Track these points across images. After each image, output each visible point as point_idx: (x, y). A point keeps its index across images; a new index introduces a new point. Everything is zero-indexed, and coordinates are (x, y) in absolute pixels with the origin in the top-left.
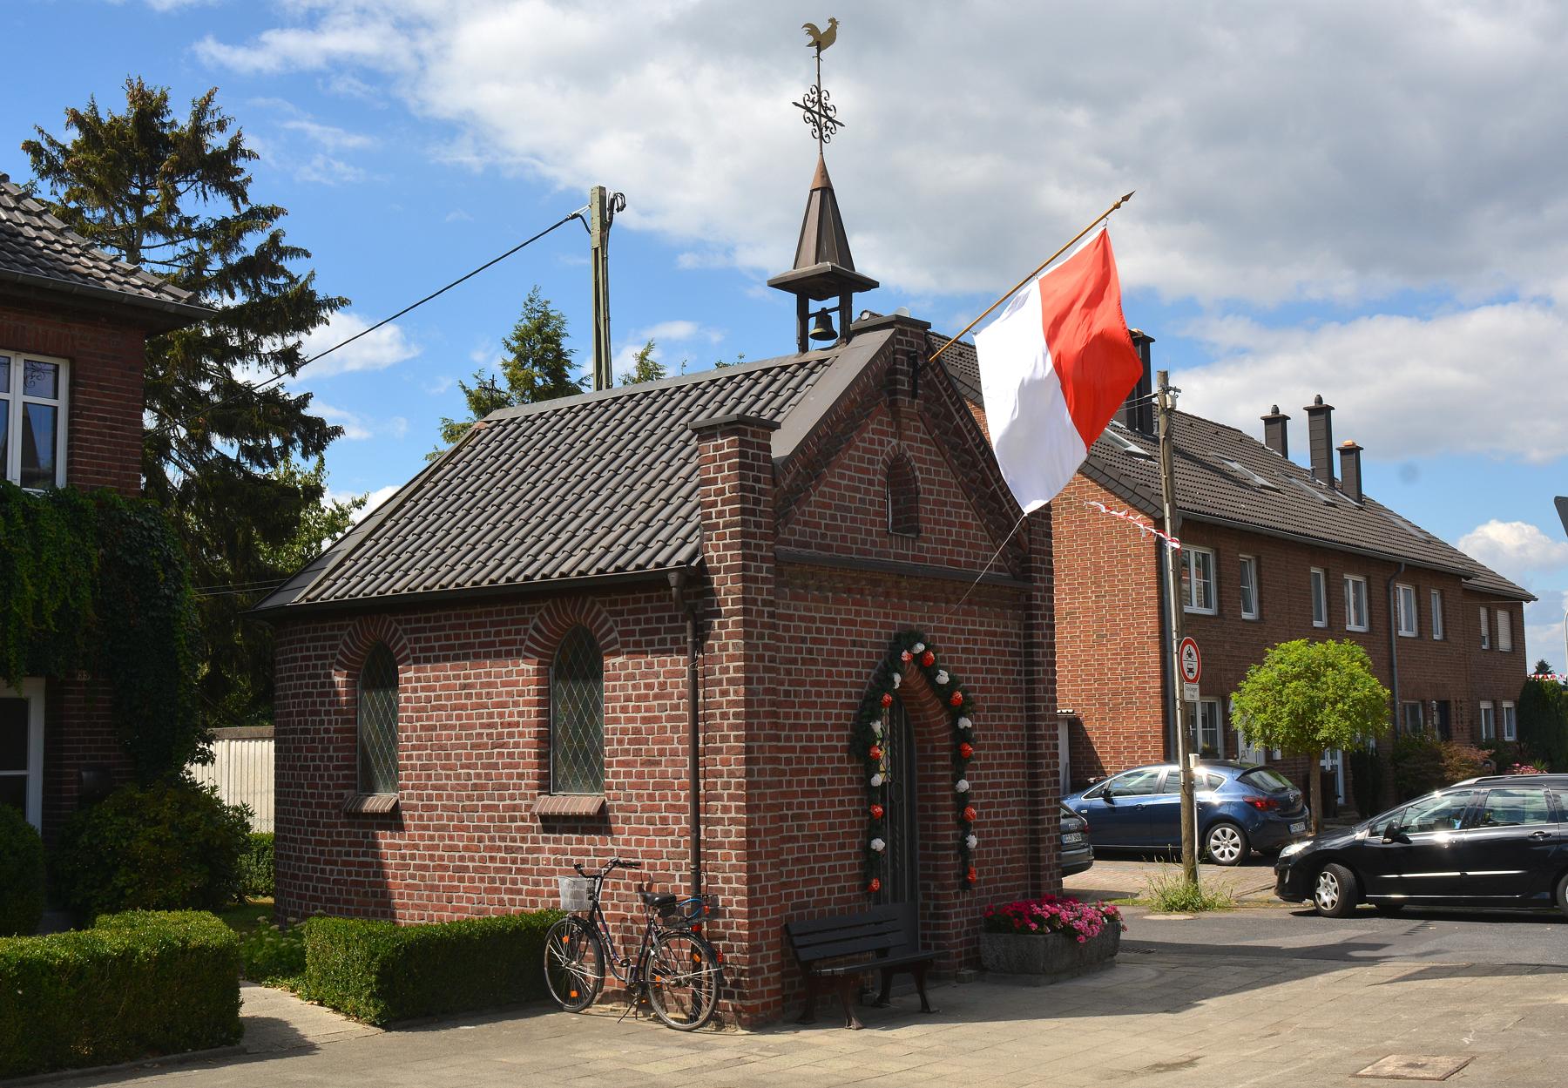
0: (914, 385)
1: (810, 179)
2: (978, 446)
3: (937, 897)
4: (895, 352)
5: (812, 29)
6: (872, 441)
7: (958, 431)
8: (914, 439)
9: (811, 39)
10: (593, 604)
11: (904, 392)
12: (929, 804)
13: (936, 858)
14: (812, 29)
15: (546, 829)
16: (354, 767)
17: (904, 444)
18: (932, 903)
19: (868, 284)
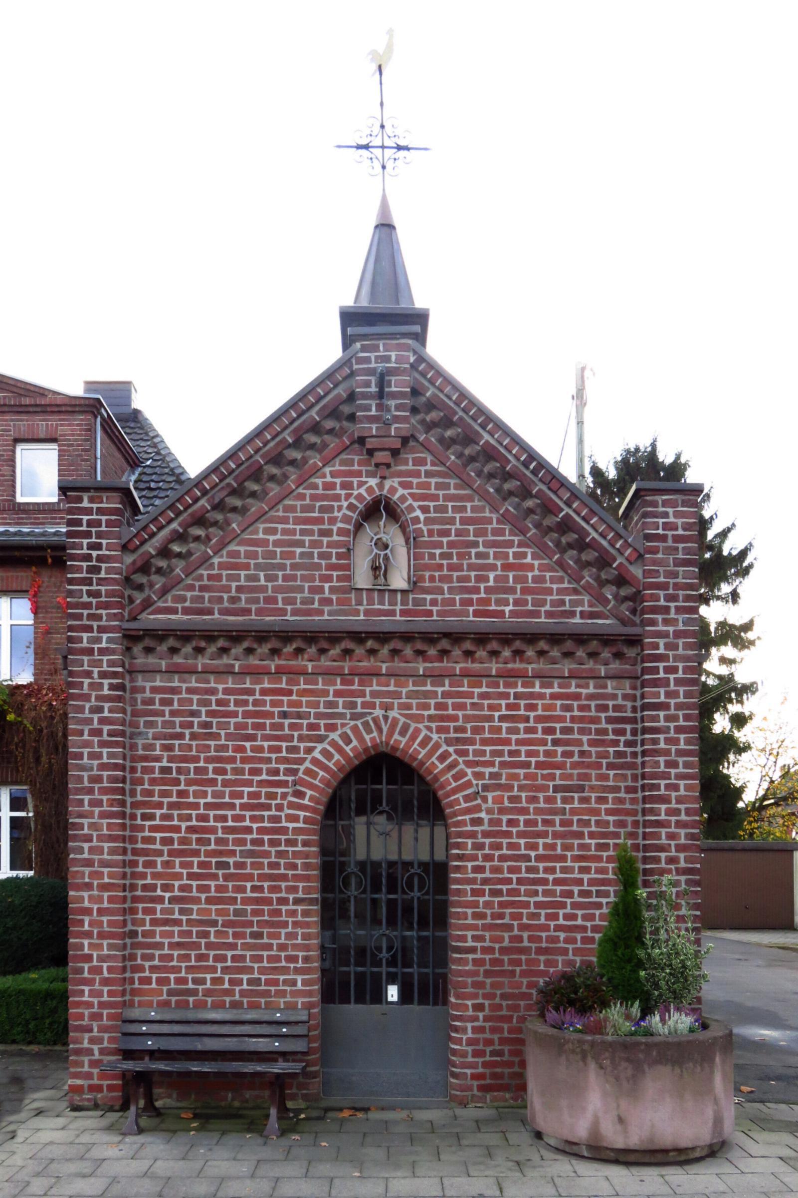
7: (489, 454)
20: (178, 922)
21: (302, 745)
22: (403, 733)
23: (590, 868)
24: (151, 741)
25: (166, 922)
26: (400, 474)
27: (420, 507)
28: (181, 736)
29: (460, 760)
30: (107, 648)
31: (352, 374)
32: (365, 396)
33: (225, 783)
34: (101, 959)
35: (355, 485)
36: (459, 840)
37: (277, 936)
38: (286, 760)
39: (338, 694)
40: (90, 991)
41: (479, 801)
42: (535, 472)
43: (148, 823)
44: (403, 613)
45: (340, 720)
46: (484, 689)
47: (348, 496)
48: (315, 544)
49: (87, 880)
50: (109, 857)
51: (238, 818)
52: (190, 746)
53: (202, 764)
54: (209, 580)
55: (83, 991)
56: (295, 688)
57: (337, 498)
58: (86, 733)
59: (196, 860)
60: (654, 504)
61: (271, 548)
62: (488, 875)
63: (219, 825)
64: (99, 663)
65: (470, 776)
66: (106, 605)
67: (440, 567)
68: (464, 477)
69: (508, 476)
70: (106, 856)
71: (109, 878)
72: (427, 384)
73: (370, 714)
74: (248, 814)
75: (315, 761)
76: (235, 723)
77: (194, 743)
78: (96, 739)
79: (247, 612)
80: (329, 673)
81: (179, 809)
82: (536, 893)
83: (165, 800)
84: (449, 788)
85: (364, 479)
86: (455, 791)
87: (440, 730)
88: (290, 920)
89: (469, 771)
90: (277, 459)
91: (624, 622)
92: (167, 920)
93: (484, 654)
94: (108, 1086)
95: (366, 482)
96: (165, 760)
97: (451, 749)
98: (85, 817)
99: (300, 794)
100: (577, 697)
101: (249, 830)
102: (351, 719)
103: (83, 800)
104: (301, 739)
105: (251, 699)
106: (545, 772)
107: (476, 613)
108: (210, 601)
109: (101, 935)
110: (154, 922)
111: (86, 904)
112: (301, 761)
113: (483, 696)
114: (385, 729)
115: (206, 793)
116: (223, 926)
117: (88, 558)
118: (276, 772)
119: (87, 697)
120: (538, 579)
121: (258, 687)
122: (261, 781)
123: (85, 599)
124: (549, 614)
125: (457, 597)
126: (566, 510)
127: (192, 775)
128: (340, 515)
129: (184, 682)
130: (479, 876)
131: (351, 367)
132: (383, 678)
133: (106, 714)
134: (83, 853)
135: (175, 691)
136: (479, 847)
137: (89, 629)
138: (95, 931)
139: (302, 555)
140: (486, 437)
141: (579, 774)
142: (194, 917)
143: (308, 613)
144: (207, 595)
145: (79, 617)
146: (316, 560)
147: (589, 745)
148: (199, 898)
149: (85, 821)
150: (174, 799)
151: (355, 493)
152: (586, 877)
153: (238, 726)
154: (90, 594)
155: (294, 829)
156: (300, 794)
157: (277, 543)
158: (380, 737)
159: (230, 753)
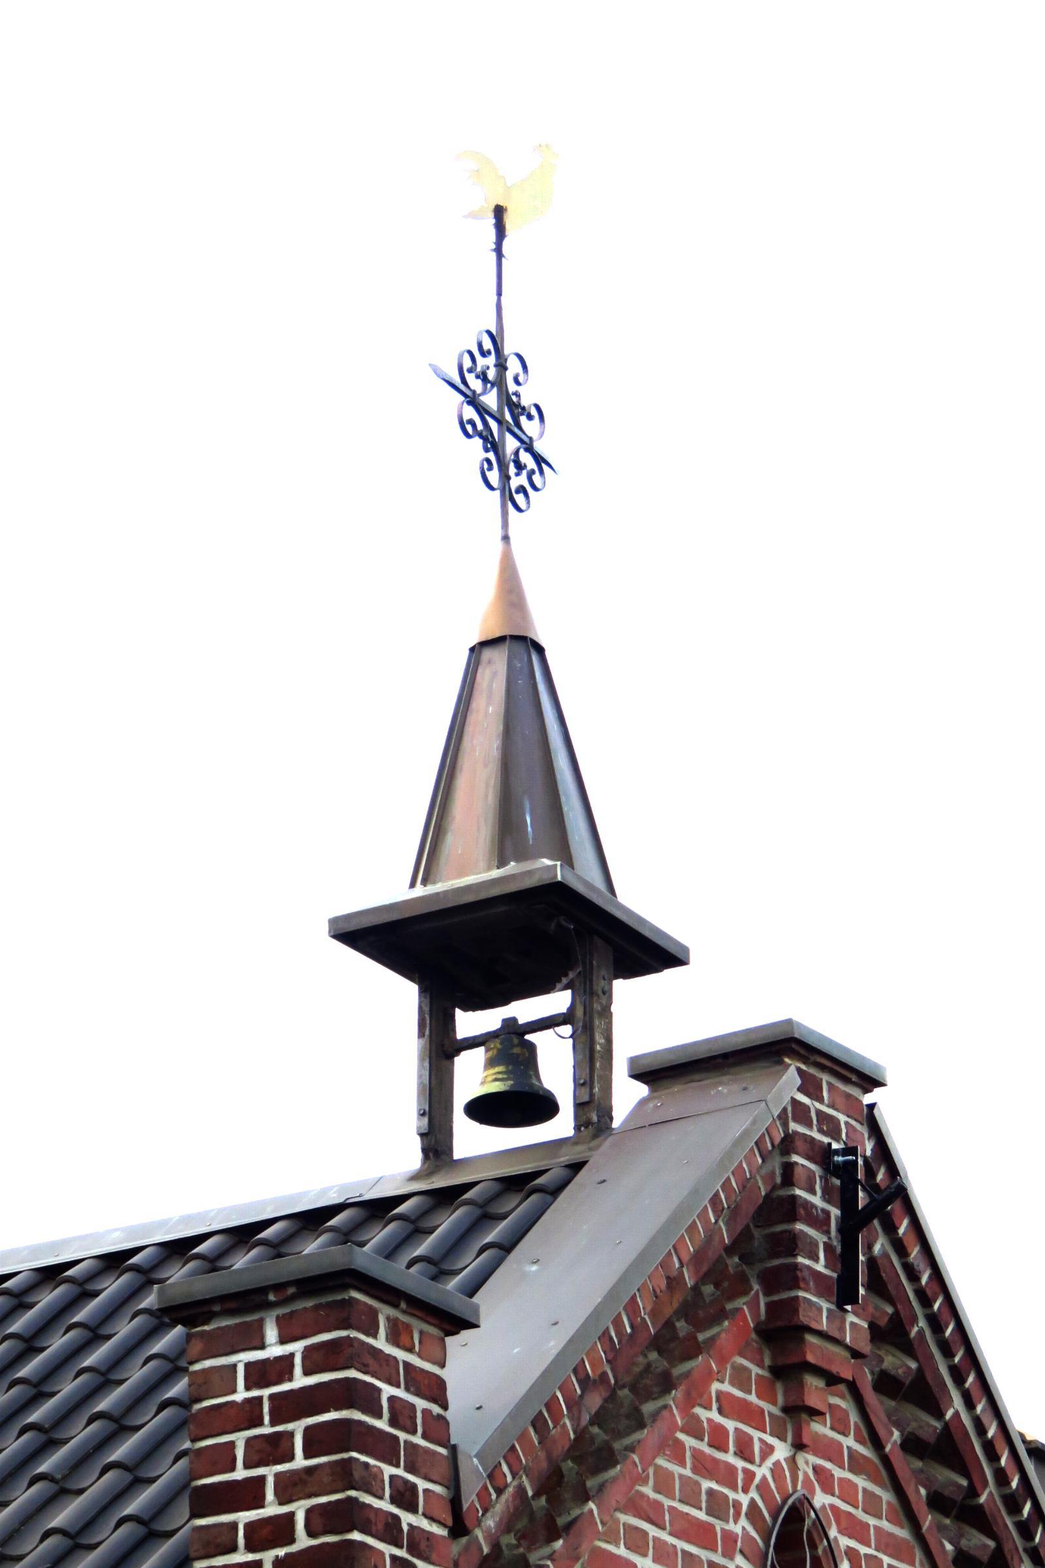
0: (845, 1259)
4: (788, 1144)
8: (831, 1452)
17: (808, 1461)
19: (649, 954)
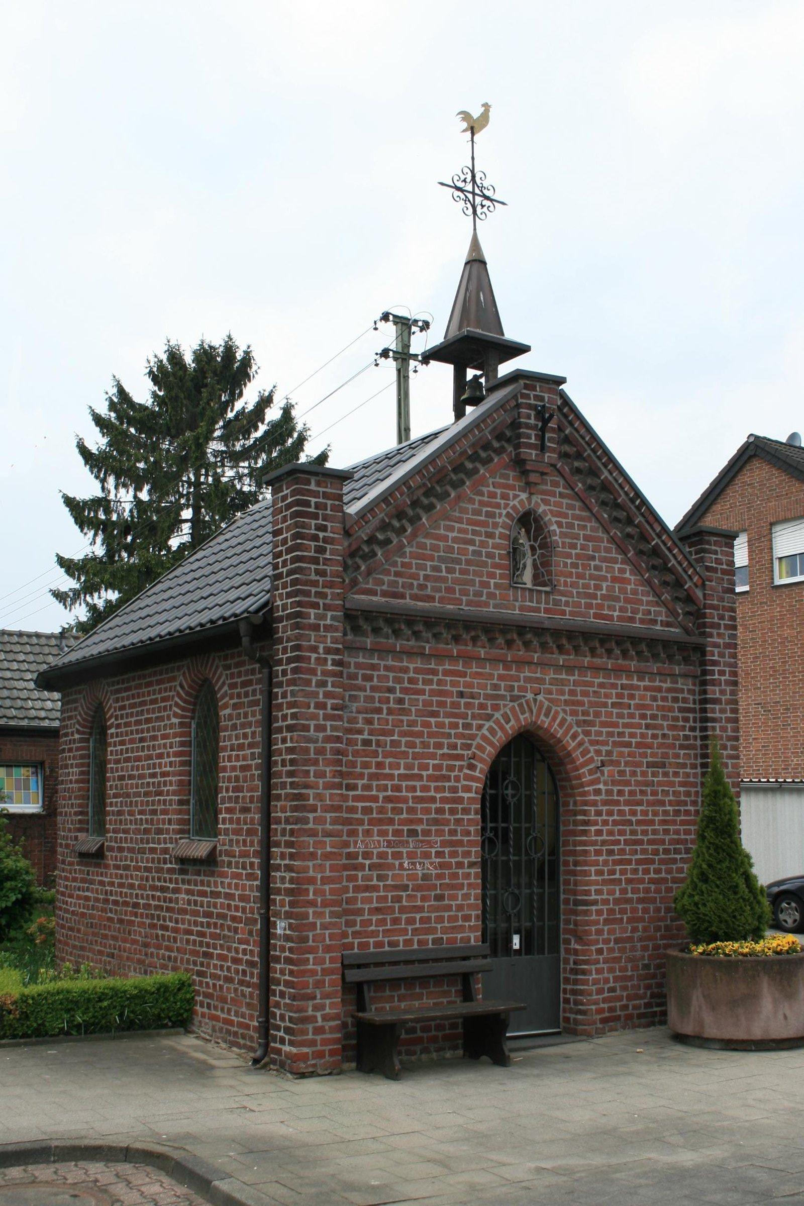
0: (542, 438)
1: (462, 254)
2: (632, 501)
3: (576, 952)
5: (466, 116)
6: (493, 495)
7: (605, 487)
9: (465, 125)
10: (214, 660)
11: (530, 446)
12: (571, 859)
13: (575, 913)
14: (466, 116)
15: (183, 872)
16: (86, 814)
18: (572, 958)
20: (375, 888)
21: (474, 723)
22: (547, 715)
23: (625, 831)
24: (354, 715)
25: (367, 888)
26: (543, 493)
27: (556, 522)
28: (379, 711)
29: (586, 739)
30: (331, 625)
31: (518, 406)
32: (528, 426)
33: (416, 756)
34: (324, 927)
35: (511, 497)
36: (586, 808)
37: (455, 897)
38: (462, 736)
39: (501, 678)
40: (314, 958)
41: (599, 774)
42: (638, 508)
43: (351, 793)
44: (547, 611)
45: (491, 702)
46: (601, 680)
47: (506, 505)
48: (483, 544)
49: (312, 850)
50: (331, 827)
51: (425, 789)
52: (387, 720)
53: (396, 737)
54: (402, 567)
55: (308, 959)
56: (469, 671)
57: (498, 506)
58: (312, 706)
59: (390, 828)
60: (709, 543)
61: (450, 543)
62: (605, 837)
63: (410, 795)
64: (323, 639)
65: (592, 754)
66: (331, 585)
67: (570, 575)
68: (587, 502)
69: (617, 506)
70: (328, 826)
71: (331, 847)
72: (566, 423)
73: (525, 696)
74: (433, 785)
75: (484, 738)
76: (423, 700)
77: (390, 718)
78: (321, 712)
79: (431, 599)
80: (494, 661)
81: (378, 780)
82: (636, 852)
83: (366, 771)
84: (578, 763)
85: (517, 493)
86: (583, 765)
87: (574, 713)
88: (466, 882)
89: (592, 749)
90: (458, 468)
91: (687, 631)
92: (367, 886)
93: (430, 635)
94: (330, 1050)
95: (519, 496)
96: (366, 733)
97: (579, 730)
98: (312, 788)
99: (472, 767)
100: (659, 689)
101: (433, 800)
102: (511, 701)
103: (309, 771)
104: (474, 717)
105: (435, 678)
106: (641, 751)
107: (596, 616)
108: (403, 587)
109: (325, 904)
110: (357, 889)
111: (311, 873)
112: (473, 737)
113: (601, 685)
114: (535, 711)
115: (399, 764)
116: (413, 890)
117: (315, 538)
118: (454, 747)
119: (313, 672)
120: (635, 592)
121: (441, 668)
122: (443, 755)
123: (313, 577)
124: (642, 621)
125: (583, 601)
126: (656, 540)
127: (388, 748)
128: (501, 521)
129: (383, 659)
130: (599, 838)
131: (517, 400)
132: (533, 667)
133: (329, 688)
134: (308, 823)
135: (374, 667)
136: (599, 813)
137: (315, 606)
138: (319, 900)
139: (474, 552)
140: (606, 473)
141: (662, 753)
142: (389, 882)
143: (479, 604)
144: (400, 580)
145: (307, 594)
146: (484, 559)
147: (668, 730)
148: (394, 865)
149: (311, 792)
150: (373, 770)
151: (512, 504)
152: (667, 838)
153: (425, 703)
154: (317, 572)
155: (468, 798)
156: (472, 767)
157: (455, 540)
158: (531, 718)
159: (419, 728)
